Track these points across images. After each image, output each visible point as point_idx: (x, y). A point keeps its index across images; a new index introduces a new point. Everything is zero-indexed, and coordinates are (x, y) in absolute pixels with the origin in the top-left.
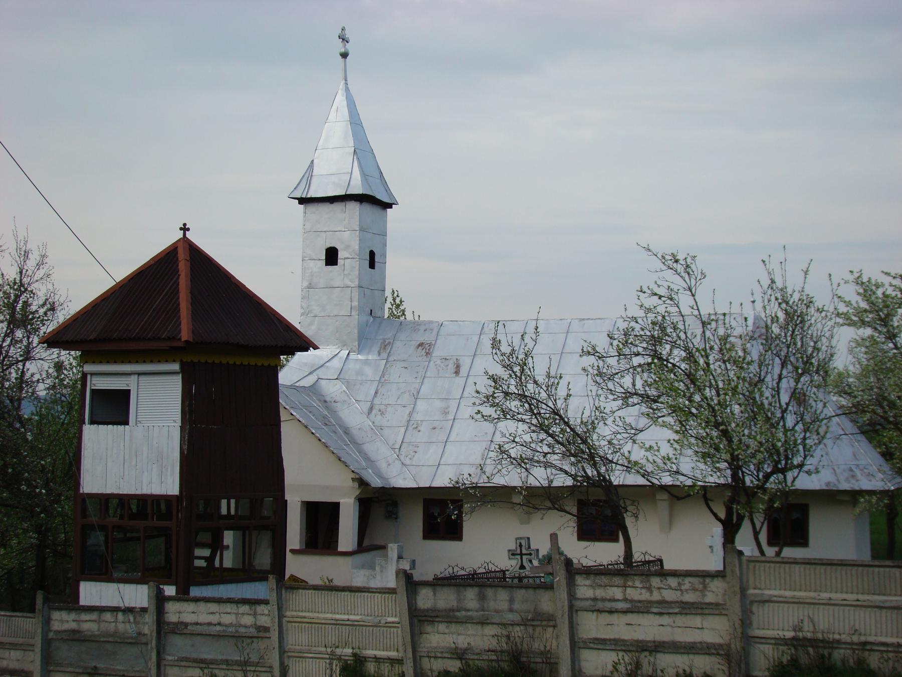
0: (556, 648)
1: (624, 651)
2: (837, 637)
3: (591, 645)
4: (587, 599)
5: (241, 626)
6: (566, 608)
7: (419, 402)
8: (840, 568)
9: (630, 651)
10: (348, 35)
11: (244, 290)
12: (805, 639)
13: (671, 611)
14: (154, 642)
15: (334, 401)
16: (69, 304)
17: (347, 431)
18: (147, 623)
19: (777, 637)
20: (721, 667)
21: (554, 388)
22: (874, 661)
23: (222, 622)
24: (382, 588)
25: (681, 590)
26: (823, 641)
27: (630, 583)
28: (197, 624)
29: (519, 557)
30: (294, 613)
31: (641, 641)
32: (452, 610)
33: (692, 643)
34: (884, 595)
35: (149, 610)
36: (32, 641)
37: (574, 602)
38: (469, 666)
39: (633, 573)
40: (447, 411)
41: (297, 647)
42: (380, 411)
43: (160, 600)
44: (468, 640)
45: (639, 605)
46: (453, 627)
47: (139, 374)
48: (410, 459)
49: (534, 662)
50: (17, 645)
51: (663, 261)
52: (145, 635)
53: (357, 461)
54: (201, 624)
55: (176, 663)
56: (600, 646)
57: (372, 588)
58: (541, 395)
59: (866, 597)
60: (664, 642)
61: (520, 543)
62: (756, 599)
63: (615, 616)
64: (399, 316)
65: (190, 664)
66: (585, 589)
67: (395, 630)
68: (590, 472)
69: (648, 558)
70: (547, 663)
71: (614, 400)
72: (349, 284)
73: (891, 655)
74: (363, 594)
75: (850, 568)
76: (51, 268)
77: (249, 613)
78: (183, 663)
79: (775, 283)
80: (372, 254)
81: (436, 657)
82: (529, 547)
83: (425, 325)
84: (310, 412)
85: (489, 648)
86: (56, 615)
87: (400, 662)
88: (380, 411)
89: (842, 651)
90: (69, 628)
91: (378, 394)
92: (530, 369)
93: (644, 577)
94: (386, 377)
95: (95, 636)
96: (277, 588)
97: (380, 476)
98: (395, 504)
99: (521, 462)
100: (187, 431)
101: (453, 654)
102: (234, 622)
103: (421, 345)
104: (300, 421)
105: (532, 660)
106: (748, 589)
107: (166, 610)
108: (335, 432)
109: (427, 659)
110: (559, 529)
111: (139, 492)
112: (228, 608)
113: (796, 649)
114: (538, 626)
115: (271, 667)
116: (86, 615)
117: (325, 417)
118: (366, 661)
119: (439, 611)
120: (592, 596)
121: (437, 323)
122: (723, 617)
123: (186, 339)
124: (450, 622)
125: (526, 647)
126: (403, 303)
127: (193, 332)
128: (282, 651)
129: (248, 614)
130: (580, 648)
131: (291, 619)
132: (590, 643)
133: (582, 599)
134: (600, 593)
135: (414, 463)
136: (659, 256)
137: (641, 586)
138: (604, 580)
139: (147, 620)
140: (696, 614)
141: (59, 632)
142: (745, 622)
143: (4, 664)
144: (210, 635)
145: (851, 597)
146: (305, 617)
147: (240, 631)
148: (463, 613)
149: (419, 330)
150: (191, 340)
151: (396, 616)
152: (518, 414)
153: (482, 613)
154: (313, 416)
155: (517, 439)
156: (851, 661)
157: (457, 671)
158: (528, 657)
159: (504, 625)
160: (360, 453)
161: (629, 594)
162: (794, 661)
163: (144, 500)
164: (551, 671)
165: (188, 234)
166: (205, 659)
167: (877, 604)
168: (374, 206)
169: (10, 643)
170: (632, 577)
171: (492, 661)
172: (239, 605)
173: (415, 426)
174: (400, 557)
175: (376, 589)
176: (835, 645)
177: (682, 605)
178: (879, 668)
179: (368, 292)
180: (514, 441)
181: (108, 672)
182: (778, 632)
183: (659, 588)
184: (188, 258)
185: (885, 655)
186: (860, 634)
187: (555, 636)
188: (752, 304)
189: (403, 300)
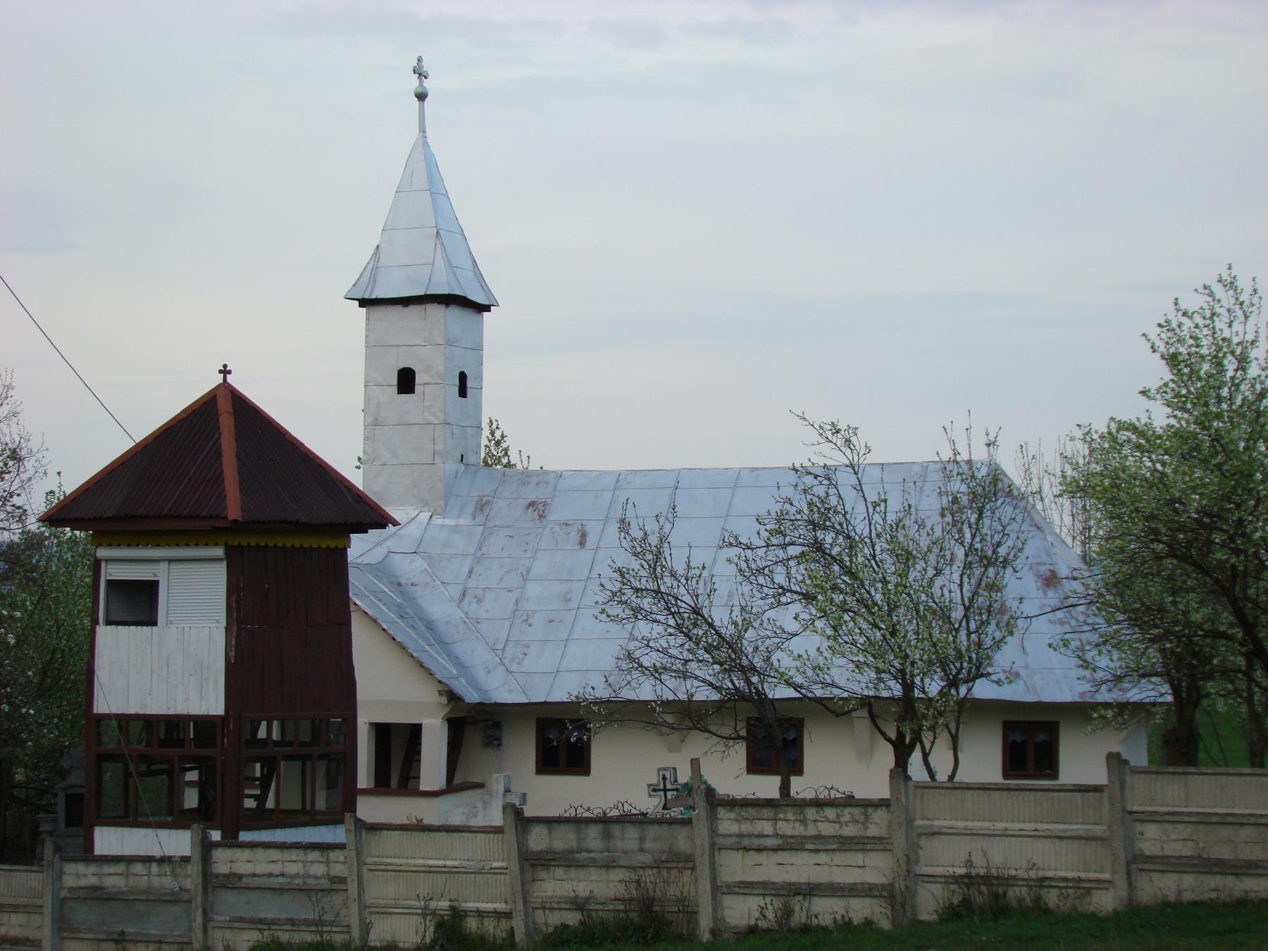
0: (694, 894)
1: (774, 895)
2: (1013, 872)
3: (737, 890)
4: (731, 836)
5: (309, 876)
6: (707, 845)
7: (529, 585)
8: (1017, 793)
9: (780, 895)
10: (426, 66)
11: (302, 449)
12: (978, 876)
13: (828, 847)
14: (199, 899)
15: (412, 584)
16: (45, 453)
17: (430, 626)
18: (190, 876)
19: (948, 874)
20: (884, 911)
21: (694, 580)
22: (1052, 898)
23: (285, 873)
24: (486, 827)
25: (839, 822)
26: (998, 878)
27: (781, 816)
28: (254, 875)
29: (662, 793)
30: (377, 860)
31: (794, 884)
32: (571, 852)
33: (853, 884)
34: (1064, 823)
36: (38, 902)
37: (716, 839)
38: (592, 917)
39: (785, 803)
40: (568, 597)
41: (381, 901)
42: (475, 597)
43: (207, 847)
44: (591, 887)
45: (792, 841)
46: (573, 872)
48: (519, 664)
51: (821, 431)
52: (186, 890)
53: (445, 667)
54: (259, 876)
55: (226, 925)
56: (748, 891)
57: (473, 827)
58: (680, 590)
59: (1045, 826)
61: (664, 775)
64: (500, 457)
65: (245, 925)
66: (728, 824)
67: (502, 877)
68: (740, 684)
70: (684, 912)
73: (1071, 891)
74: (463, 834)
75: (1028, 793)
76: (18, 403)
78: (237, 925)
79: (959, 454)
80: (463, 377)
81: (552, 909)
82: (676, 781)
84: (380, 600)
85: (615, 895)
86: (70, 868)
87: (508, 915)
88: (476, 597)
89: (1017, 889)
92: (665, 558)
93: (797, 808)
94: (484, 550)
95: (122, 893)
96: (355, 829)
97: (477, 688)
98: (497, 725)
99: (656, 672)
100: (234, 634)
101: (573, 904)
102: (301, 872)
103: (532, 504)
104: (366, 613)
105: (667, 909)
106: (915, 820)
107: (214, 859)
108: (415, 628)
109: (541, 911)
111: (171, 712)
112: (293, 854)
114: (673, 868)
116: (110, 867)
117: (399, 607)
118: (466, 916)
119: (555, 853)
122: (887, 853)
124: (570, 866)
126: (505, 439)
127: (242, 509)
128: (363, 907)
129: (319, 862)
130: (723, 893)
131: (373, 867)
132: (735, 887)
133: (725, 836)
134: (746, 827)
135: (523, 669)
137: (794, 818)
138: (752, 812)
139: (189, 872)
140: (857, 850)
141: (75, 889)
142: (911, 859)
143: (1, 931)
146: (391, 864)
147: (308, 882)
148: (585, 855)
150: (241, 519)
151: (503, 861)
152: (651, 613)
153: (607, 854)
154: (384, 605)
155: (652, 644)
156: (1028, 899)
157: (577, 925)
159: (633, 868)
160: (448, 655)
161: (780, 828)
162: (966, 902)
164: (689, 923)
165: (230, 379)
166: (266, 919)
167: (1057, 834)
168: (465, 309)
170: (784, 808)
171: (618, 911)
172: (307, 851)
173: (524, 618)
174: (507, 791)
175: (479, 827)
176: (1011, 882)
177: (841, 839)
178: (1058, 907)
180: (648, 646)
181: (139, 938)
182: (948, 868)
183: (815, 821)
184: (231, 411)
185: (1063, 891)
186: (1038, 869)
187: (693, 880)
188: (986, 448)
189: (505, 434)
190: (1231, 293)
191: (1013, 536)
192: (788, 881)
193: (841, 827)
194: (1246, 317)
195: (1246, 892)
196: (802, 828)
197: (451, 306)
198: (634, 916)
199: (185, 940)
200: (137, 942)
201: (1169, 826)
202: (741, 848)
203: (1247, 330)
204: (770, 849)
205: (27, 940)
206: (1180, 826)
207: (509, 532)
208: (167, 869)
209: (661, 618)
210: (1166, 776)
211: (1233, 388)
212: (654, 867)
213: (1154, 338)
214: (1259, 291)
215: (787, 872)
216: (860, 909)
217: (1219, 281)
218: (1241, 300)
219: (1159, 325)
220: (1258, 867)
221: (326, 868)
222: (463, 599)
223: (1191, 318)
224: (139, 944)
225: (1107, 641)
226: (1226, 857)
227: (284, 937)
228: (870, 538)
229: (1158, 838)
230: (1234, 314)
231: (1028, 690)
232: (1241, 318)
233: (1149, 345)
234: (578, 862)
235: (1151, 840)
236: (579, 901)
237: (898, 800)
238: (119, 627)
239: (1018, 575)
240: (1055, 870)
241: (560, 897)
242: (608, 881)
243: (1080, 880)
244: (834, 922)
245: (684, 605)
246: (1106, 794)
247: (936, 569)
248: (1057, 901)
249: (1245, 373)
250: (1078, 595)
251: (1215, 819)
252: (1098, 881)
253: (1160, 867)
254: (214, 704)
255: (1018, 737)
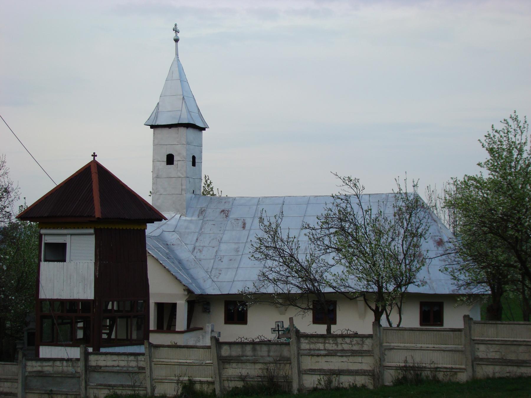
1: (324, 375)
2: (424, 365)
4: (306, 350)
5: (130, 367)
6: (296, 354)
7: (222, 245)
9: (327, 375)
10: (178, 28)
11: (127, 188)
12: (410, 366)
13: (347, 354)
14: (83, 376)
15: (172, 245)
16: (19, 190)
17: (180, 262)
18: (79, 367)
19: (397, 366)
20: (370, 381)
21: (291, 243)
22: (440, 376)
24: (204, 346)
25: (352, 344)
26: (418, 367)
27: (327, 341)
28: (106, 366)
29: (277, 332)
30: (158, 360)
31: (332, 370)
32: (239, 356)
34: (446, 344)
35: (80, 360)
37: (300, 351)
38: (248, 384)
39: (329, 336)
41: (160, 377)
43: (86, 355)
45: (332, 352)
46: (240, 365)
47: (71, 235)
49: (280, 382)
50: (8, 379)
51: (344, 180)
52: (78, 373)
53: (186, 279)
54: (108, 366)
55: (95, 387)
60: (343, 370)
61: (278, 325)
62: (387, 348)
63: (320, 357)
64: (209, 191)
66: (305, 345)
67: (210, 367)
68: (310, 286)
69: (349, 332)
70: (286, 382)
71: (319, 250)
72: (181, 175)
73: (449, 373)
74: (194, 349)
76: (7, 169)
77: (134, 360)
78: (99, 387)
79: (402, 190)
80: (194, 158)
81: (231, 380)
82: (283, 327)
83: (225, 199)
84: (159, 251)
86: (29, 363)
87: (213, 383)
88: (199, 250)
89: (426, 372)
90: (37, 370)
91: (198, 240)
92: (278, 234)
93: (334, 338)
94: (203, 230)
97: (200, 288)
98: (208, 304)
99: (275, 281)
100: (98, 265)
101: (240, 378)
103: (223, 211)
104: (153, 257)
105: (279, 380)
107: (90, 359)
110: (295, 315)
111: (72, 298)
112: (123, 358)
113: (406, 372)
114: (282, 363)
115: (146, 388)
116: (46, 363)
118: (195, 383)
119: (232, 357)
120: (309, 348)
121: (232, 198)
123: (98, 217)
124: (238, 363)
125: (276, 374)
126: (211, 184)
127: (101, 213)
128: (152, 379)
130: (303, 374)
131: (156, 363)
132: (308, 371)
133: (304, 350)
134: (312, 346)
135: (219, 280)
136: (342, 178)
137: (332, 343)
138: (315, 340)
139: (79, 365)
140: (359, 356)
141: (31, 372)
142: (381, 360)
143: (1, 390)
144: (113, 372)
145: (430, 346)
147: (129, 369)
148: (245, 358)
149: (221, 202)
151: (210, 360)
152: (273, 256)
154: (161, 253)
155: (273, 269)
156: (430, 376)
158: (277, 379)
160: (188, 274)
161: (327, 347)
162: (405, 378)
163: (73, 303)
164: (288, 386)
166: (111, 384)
167: (443, 349)
169: (4, 379)
171: (259, 381)
172: (129, 356)
173: (219, 259)
174: (212, 331)
175: (201, 346)
176: (424, 369)
177: (352, 351)
178: (443, 380)
179: (191, 180)
180: (271, 270)
181: (58, 393)
182: (397, 363)
183: (341, 344)
184: (97, 172)
185: (445, 373)
186: (435, 364)
189: (211, 182)
190: (516, 122)
191: (424, 224)
192: (330, 369)
193: (352, 346)
194: (522, 133)
195: (522, 373)
196: (336, 346)
197: (189, 128)
198: (265, 383)
199: (78, 393)
200: (57, 394)
201: (489, 346)
202: (310, 355)
203: (522, 138)
204: (322, 355)
205: (11, 393)
206: (494, 346)
207: (213, 223)
208: (70, 363)
209: (277, 259)
210: (488, 325)
211: (516, 162)
212: (274, 363)
213: (483, 141)
214: (527, 122)
215: (330, 365)
216: (360, 381)
217: (511, 118)
218: (520, 125)
219: (486, 136)
220: (527, 363)
221: (136, 363)
222: (194, 251)
223: (499, 133)
224: (58, 395)
225: (464, 268)
226: (513, 358)
227: (119, 392)
228: (364, 225)
229: (485, 351)
230: (517, 132)
231: (431, 289)
232: (520, 133)
233: (481, 144)
234: (242, 361)
235: (482, 351)
236: (243, 377)
237: (376, 335)
238: (51, 263)
239: (427, 241)
240: (442, 364)
241: (235, 376)
242: (255, 369)
243: (452, 368)
244: (349, 386)
245: (286, 253)
246: (463, 333)
247: (392, 238)
248: (443, 377)
249: (522, 156)
250: (452, 249)
251: (509, 343)
252: (460, 369)
253: (485, 363)
254: (89, 294)
255: (426, 309)
